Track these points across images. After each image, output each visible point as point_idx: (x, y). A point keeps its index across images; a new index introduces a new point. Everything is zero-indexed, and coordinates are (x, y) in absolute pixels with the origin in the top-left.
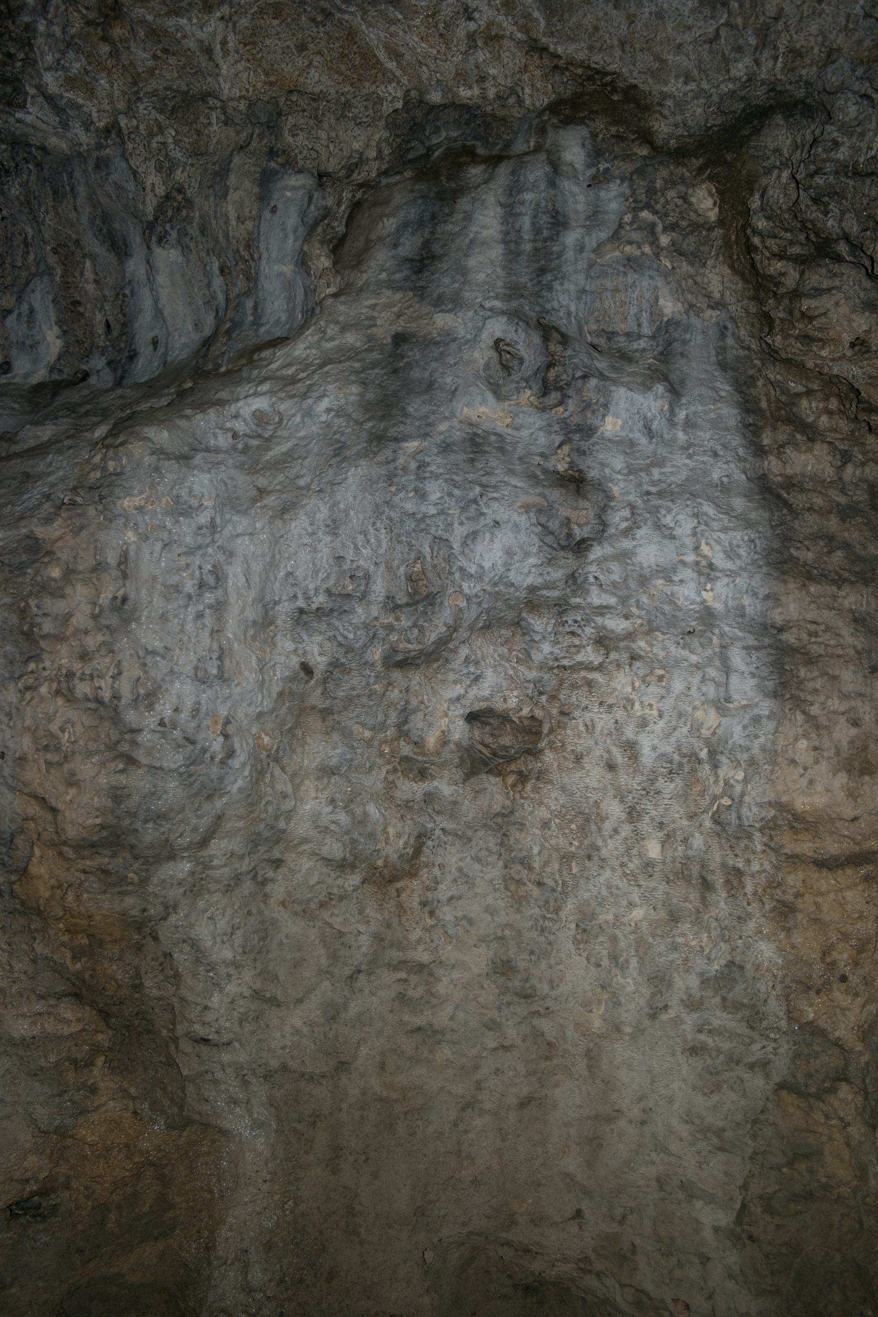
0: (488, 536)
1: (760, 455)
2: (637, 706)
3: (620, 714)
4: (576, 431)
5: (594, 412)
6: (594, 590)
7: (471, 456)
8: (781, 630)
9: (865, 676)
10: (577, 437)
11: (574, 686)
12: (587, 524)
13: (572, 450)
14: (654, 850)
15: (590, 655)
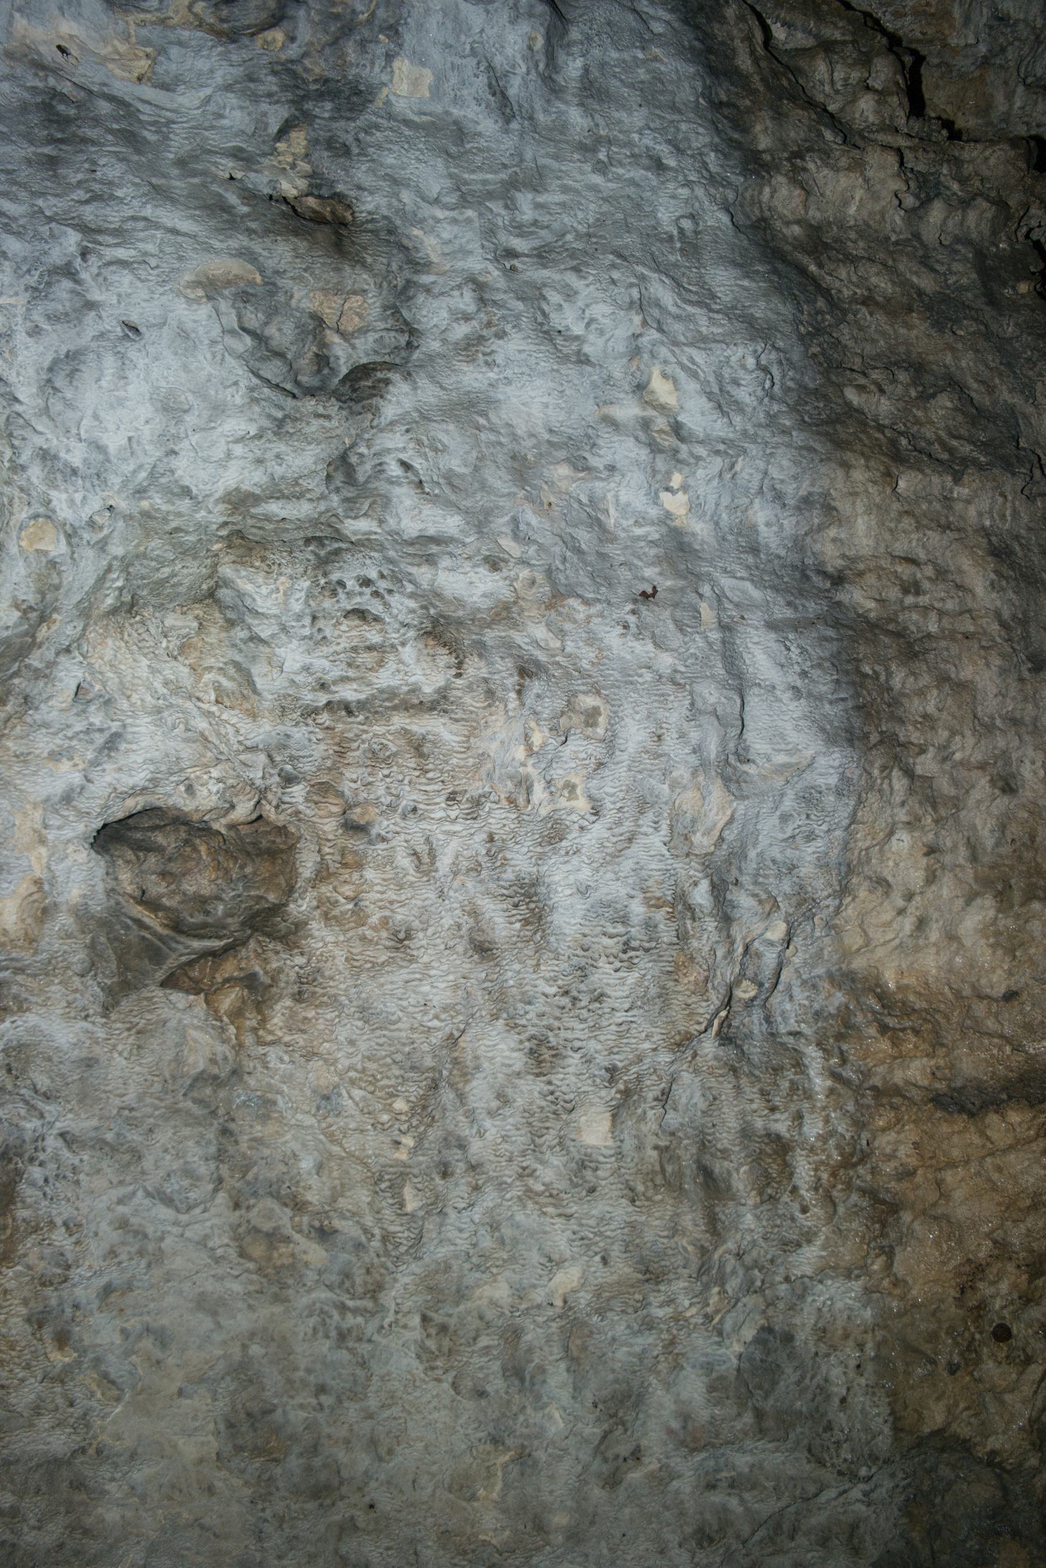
0: (110, 362)
1: (753, 172)
2: (539, 793)
3: (498, 818)
4: (321, 96)
5: (363, 44)
6: (404, 497)
7: (47, 150)
8: (838, 580)
9: (1021, 680)
10: (325, 109)
11: (377, 758)
12: (363, 331)
13: (314, 142)
14: (594, 1131)
15: (419, 669)
